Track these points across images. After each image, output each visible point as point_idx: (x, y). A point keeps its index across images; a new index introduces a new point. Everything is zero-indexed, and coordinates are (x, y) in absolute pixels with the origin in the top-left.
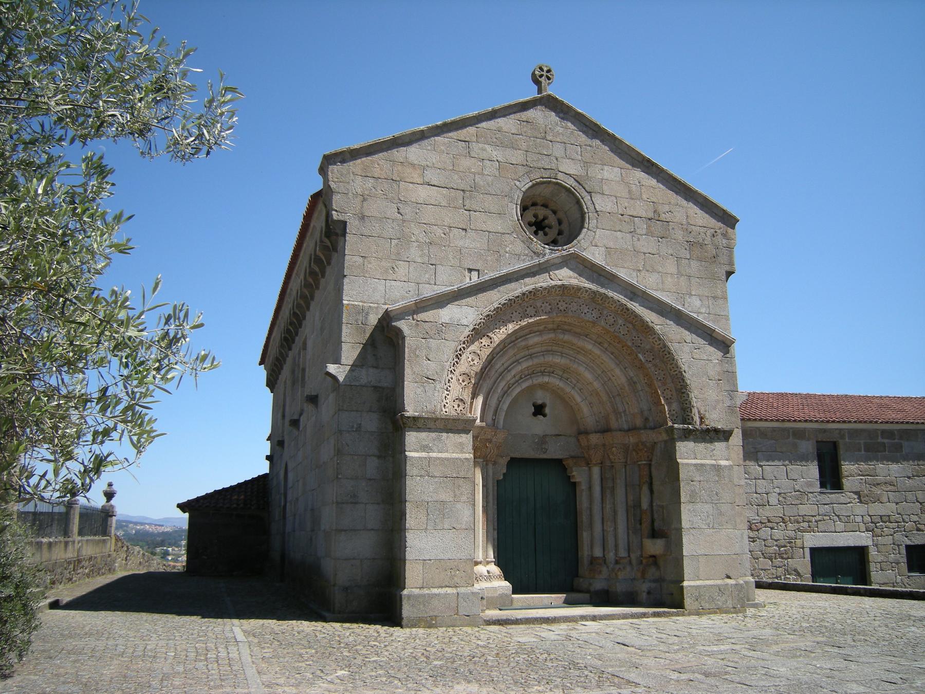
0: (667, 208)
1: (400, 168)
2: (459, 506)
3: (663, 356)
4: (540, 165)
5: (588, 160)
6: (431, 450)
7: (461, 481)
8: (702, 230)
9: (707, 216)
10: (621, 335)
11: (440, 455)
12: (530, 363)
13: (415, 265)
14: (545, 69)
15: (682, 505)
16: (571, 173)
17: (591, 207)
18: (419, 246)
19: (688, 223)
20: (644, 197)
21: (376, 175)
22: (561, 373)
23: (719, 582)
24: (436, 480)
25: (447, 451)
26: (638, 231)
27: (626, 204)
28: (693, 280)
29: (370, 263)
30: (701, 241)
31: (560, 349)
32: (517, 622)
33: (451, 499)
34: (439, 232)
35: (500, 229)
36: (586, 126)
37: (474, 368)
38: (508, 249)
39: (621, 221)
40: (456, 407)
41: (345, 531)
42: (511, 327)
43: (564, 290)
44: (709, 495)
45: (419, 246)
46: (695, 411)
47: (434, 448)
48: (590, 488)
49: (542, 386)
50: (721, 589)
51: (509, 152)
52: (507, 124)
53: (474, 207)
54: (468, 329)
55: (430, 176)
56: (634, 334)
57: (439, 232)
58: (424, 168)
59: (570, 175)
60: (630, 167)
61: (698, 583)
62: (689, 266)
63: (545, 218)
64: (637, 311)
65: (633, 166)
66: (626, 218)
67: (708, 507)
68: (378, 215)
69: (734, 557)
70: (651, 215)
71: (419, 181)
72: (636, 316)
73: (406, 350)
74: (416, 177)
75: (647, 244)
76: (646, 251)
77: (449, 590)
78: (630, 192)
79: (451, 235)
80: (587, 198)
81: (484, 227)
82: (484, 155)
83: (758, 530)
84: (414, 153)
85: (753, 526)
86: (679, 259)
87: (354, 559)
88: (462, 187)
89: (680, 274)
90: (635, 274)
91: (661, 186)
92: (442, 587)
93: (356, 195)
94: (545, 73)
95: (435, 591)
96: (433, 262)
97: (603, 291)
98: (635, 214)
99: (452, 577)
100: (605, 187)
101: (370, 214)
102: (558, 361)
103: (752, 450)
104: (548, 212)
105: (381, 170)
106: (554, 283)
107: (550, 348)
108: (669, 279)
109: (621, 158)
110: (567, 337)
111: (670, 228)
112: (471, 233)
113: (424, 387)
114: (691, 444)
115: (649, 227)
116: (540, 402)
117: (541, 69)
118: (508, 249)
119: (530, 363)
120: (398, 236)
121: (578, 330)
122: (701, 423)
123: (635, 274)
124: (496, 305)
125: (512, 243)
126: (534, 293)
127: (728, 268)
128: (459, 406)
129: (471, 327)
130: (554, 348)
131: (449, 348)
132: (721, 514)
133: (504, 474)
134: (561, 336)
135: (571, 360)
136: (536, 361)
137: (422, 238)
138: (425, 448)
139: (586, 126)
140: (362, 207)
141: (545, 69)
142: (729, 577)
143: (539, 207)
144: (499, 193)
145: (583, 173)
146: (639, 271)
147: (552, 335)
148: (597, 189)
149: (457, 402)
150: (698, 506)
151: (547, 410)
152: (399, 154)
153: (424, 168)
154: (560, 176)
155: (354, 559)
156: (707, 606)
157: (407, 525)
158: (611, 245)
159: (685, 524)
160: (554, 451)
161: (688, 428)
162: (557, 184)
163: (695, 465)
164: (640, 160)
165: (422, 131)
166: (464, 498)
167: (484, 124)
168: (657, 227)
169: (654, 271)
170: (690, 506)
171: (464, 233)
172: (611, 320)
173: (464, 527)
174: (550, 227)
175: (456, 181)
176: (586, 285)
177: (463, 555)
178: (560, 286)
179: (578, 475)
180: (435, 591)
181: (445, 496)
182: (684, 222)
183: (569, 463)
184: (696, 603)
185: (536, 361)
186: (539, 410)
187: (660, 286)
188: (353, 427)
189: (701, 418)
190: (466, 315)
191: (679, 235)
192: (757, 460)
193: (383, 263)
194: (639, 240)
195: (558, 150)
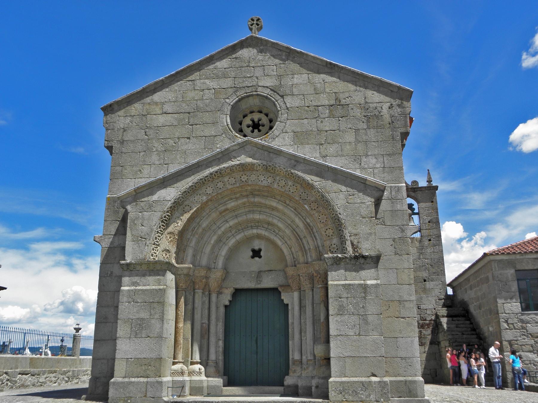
0: (347, 95)
1: (148, 107)
2: (153, 321)
3: (324, 203)
4: (244, 85)
5: (281, 74)
6: (139, 285)
7: (155, 305)
8: (378, 105)
10: (290, 193)
11: (144, 288)
12: (236, 221)
13: (154, 166)
14: (255, 20)
16: (268, 85)
17: (283, 106)
18: (157, 154)
19: (366, 103)
20: (327, 90)
21: (133, 114)
22: (266, 226)
23: (363, 379)
24: (139, 304)
25: (149, 285)
26: (322, 116)
27: (312, 98)
29: (126, 169)
30: (377, 113)
31: (259, 209)
33: (148, 317)
34: (171, 142)
35: (213, 133)
36: (281, 50)
37: (178, 228)
38: (218, 146)
40: (164, 255)
41: (99, 340)
43: (243, 167)
44: (355, 309)
45: (157, 154)
47: (141, 283)
48: (293, 308)
49: (259, 237)
51: (222, 80)
52: (223, 64)
53: (196, 122)
54: (170, 203)
55: (168, 108)
56: (302, 191)
57: (171, 142)
58: (163, 104)
59: (267, 87)
61: (344, 379)
62: (366, 134)
63: (253, 121)
66: (312, 108)
68: (132, 138)
69: (380, 358)
70: (333, 102)
71: (159, 112)
72: (299, 177)
73: (129, 221)
74: (158, 110)
75: (328, 124)
76: (327, 129)
77: (142, 380)
78: (315, 89)
79: (179, 143)
80: (280, 100)
81: (202, 134)
82: (204, 87)
84: (157, 97)
86: (357, 130)
87: (103, 359)
88: (188, 111)
89: (357, 141)
90: (318, 147)
92: (138, 377)
93: (118, 130)
94: (255, 22)
95: (133, 380)
96: (167, 163)
98: (319, 104)
100: (294, 90)
101: (127, 139)
102: (258, 217)
104: (262, 116)
105: (136, 110)
107: (251, 209)
108: (348, 147)
110: (257, 199)
111: (349, 109)
112: (193, 140)
113: (139, 244)
115: (330, 111)
117: (253, 20)
118: (218, 146)
119: (236, 221)
120: (145, 149)
121: (266, 194)
123: (318, 147)
125: (222, 141)
127: (403, 130)
128: (166, 254)
129: (173, 201)
130: (255, 209)
131: (155, 218)
133: (230, 301)
134: (252, 200)
135: (267, 216)
136: (240, 219)
137: (160, 148)
138: (135, 284)
139: (281, 50)
140: (123, 136)
141: (255, 20)
142: (374, 375)
143: (249, 115)
144: (214, 109)
145: (277, 83)
146: (322, 144)
147: (245, 200)
148: (288, 92)
149: (165, 252)
151: (262, 253)
153: (163, 104)
155: (103, 359)
157: (118, 335)
158: (299, 130)
160: (267, 283)
162: (258, 95)
163: (343, 285)
164: (325, 64)
165: (162, 80)
166: (157, 316)
168: (339, 111)
169: (334, 142)
170: (338, 318)
171: (188, 140)
172: (283, 183)
173: (155, 335)
174: (263, 126)
175: (185, 107)
177: (154, 355)
178: (238, 165)
179: (285, 298)
180: (133, 380)
181: (144, 315)
182: (363, 102)
183: (280, 289)
184: (340, 395)
185: (240, 219)
186: (256, 253)
187: (340, 153)
188: (108, 274)
191: (358, 112)
193: (134, 168)
194: (322, 122)
195: (258, 72)
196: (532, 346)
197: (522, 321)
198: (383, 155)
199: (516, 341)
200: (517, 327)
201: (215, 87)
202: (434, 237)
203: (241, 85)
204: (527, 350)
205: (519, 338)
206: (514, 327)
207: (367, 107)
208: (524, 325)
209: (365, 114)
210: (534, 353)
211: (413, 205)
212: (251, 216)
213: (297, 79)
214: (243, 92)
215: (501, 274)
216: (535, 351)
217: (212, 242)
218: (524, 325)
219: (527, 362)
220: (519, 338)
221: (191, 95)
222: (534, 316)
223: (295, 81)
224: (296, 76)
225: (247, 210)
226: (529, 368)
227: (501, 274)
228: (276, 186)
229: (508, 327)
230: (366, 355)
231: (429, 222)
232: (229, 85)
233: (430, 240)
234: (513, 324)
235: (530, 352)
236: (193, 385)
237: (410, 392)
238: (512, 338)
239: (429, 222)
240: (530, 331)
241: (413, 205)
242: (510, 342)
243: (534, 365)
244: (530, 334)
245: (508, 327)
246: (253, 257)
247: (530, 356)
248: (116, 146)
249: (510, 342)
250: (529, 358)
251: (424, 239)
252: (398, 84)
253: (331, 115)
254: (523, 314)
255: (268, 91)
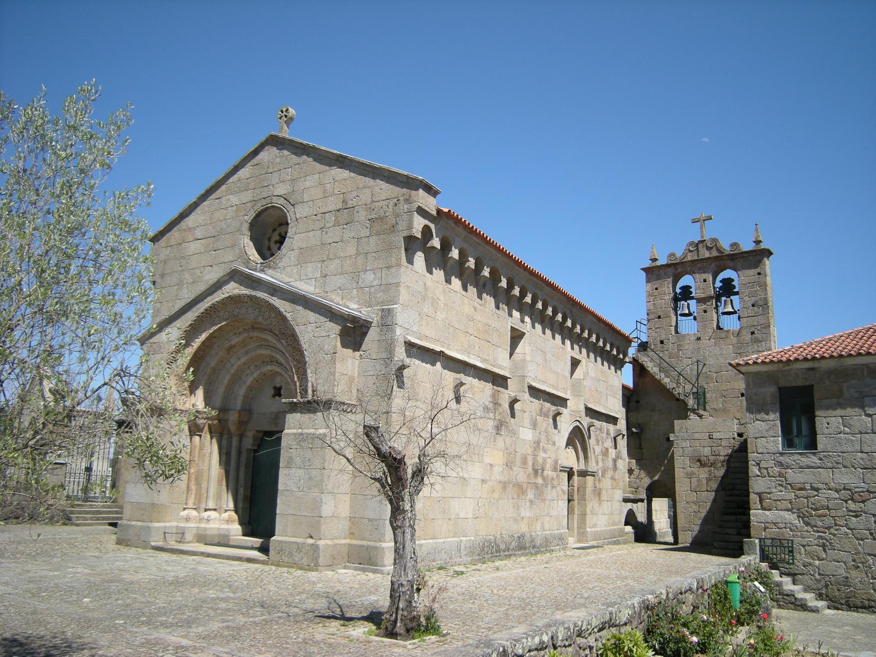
8: (385, 203)
9: (392, 186)
15: (281, 470)
20: (336, 192)
28: (369, 257)
32: (209, 555)
39: (314, 221)
42: (204, 336)
43: (233, 300)
46: (310, 385)
50: (299, 547)
52: (243, 173)
60: (327, 168)
64: (275, 304)
65: (330, 166)
66: (319, 216)
67: (300, 472)
70: (340, 206)
78: (324, 192)
81: (223, 260)
83: (863, 502)
85: (856, 496)
91: (352, 174)
97: (253, 293)
98: (326, 211)
99: (143, 515)
103: (856, 395)
106: (224, 296)
108: (348, 262)
109: (321, 163)
114: (297, 416)
116: (278, 386)
122: (313, 396)
124: (190, 322)
126: (213, 307)
132: (310, 478)
142: (311, 537)
146: (324, 261)
147: (246, 335)
150: (293, 471)
152: (183, 224)
154: (275, 199)
156: (286, 559)
159: (281, 487)
161: (292, 402)
167: (231, 180)
176: (244, 292)
180: (133, 523)
185: (250, 355)
189: (313, 391)
190: (173, 334)
192: (862, 407)
196: (790, 503)
197: (780, 464)
198: (381, 268)
199: (769, 493)
200: (771, 474)
201: (236, 206)
202: (759, 328)
203: (259, 197)
204: (784, 507)
205: (774, 490)
206: (768, 473)
207: (373, 207)
208: (783, 471)
209: (370, 217)
210: (793, 513)
211: (733, 280)
212: (259, 352)
213: (310, 181)
214: (260, 205)
215: (755, 394)
216: (795, 510)
217: (226, 382)
218: (783, 471)
219: (781, 525)
220: (774, 490)
221: (218, 215)
222: (799, 457)
223: (307, 184)
224: (308, 178)
225: (256, 344)
226: (783, 534)
227: (755, 394)
228: (260, 319)
229: (759, 473)
230: (305, 514)
231: (753, 305)
232: (249, 200)
233: (753, 333)
234: (766, 469)
235: (788, 510)
236: (200, 532)
237: (370, 559)
238: (763, 490)
239: (753, 305)
240: (790, 480)
241: (733, 280)
242: (759, 495)
243: (791, 530)
244: (790, 484)
245: (759, 473)
246: (274, 396)
247: (787, 516)
248: (158, 280)
249: (759, 495)
250: (785, 519)
251: (744, 332)
252: (406, 173)
253: (337, 224)
254: (781, 454)
255: (282, 201)
